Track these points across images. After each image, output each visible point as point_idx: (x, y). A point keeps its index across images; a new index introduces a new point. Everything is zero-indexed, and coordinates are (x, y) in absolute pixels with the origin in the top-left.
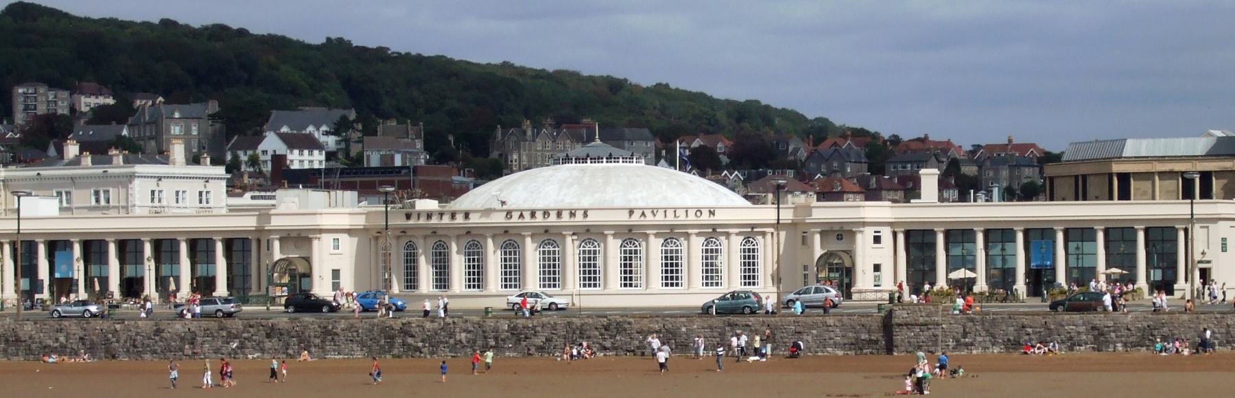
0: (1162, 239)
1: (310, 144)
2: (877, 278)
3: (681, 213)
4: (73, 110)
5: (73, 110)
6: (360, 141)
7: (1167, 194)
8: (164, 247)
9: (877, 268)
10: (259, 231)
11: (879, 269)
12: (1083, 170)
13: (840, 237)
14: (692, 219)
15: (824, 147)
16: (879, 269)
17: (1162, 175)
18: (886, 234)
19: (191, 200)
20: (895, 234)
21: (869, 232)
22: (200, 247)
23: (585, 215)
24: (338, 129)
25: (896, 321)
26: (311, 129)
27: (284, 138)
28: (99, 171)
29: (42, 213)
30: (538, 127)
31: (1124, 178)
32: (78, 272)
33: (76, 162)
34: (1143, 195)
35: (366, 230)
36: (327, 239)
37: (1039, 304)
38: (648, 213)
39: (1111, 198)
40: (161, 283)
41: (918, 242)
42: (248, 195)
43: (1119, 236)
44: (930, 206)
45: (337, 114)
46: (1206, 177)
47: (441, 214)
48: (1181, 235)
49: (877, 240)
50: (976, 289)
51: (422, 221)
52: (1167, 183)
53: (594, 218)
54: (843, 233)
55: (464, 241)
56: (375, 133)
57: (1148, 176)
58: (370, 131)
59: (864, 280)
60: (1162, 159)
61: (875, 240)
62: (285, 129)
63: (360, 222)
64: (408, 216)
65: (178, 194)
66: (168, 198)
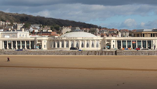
0: (150, 42)
1: (36, 29)
2: (114, 46)
3: (89, 38)
5: (5, 24)
6: (42, 28)
7: (149, 36)
8: (23, 42)
9: (114, 45)
10: (35, 40)
11: (114, 44)
12: (138, 33)
14: (85, 39)
15: (101, 30)
16: (114, 44)
17: (148, 34)
18: (115, 41)
20: (116, 41)
22: (28, 42)
23: (77, 38)
24: (40, 27)
25: (117, 52)
26: (36, 27)
27: (33, 28)
28: (13, 32)
29: (7, 37)
30: (65, 27)
31: (144, 34)
33: (10, 31)
34: (146, 37)
37: (15, 50)
38: (85, 38)
39: (142, 37)
40: (22, 46)
41: (119, 42)
42: (31, 35)
43: (144, 42)
44: (119, 37)
45: (39, 25)
46: (154, 34)
47: (58, 38)
48: (152, 41)
49: (114, 42)
51: (56, 39)
52: (149, 34)
53: (78, 39)
54: (109, 41)
55: (57, 41)
57: (147, 34)
58: (44, 27)
59: (112, 47)
60: (148, 32)
61: (113, 41)
62: (33, 27)
63: (48, 39)
64: (54, 38)
65: (24, 35)
66: (22, 36)
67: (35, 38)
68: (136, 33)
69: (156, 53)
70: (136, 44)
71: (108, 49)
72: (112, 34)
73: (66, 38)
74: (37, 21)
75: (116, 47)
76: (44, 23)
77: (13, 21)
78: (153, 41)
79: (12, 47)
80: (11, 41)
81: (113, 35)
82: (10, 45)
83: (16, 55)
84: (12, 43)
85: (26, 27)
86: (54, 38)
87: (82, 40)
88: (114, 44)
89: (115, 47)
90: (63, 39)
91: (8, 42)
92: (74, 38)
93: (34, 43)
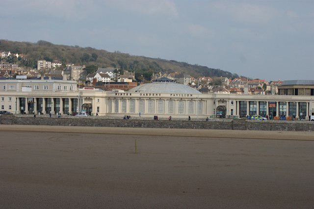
1: (107, 76)
3: (184, 95)
4: (52, 67)
5: (52, 67)
7: (307, 94)
9: (232, 110)
12: (286, 87)
13: (223, 102)
19: (68, 88)
21: (230, 101)
27: (100, 74)
31: (296, 90)
32: (52, 106)
33: (40, 78)
35: (106, 97)
36: (96, 99)
42: (84, 88)
48: (308, 104)
49: (232, 103)
50: (296, 117)
53: (162, 95)
56: (123, 74)
59: (228, 113)
62: (101, 72)
67: (81, 93)
68: (282, 88)
69: (310, 127)
70: (276, 108)
71: (221, 117)
72: (251, 89)
73: (138, 95)
74: (114, 62)
75: (236, 113)
76: (128, 66)
77: (68, 60)
78: (309, 103)
79: (35, 110)
80: (34, 99)
81: (254, 91)
82: (30, 105)
83: (247, 132)
84: (35, 101)
85: (88, 73)
86: (116, 94)
87: (171, 98)
88: (234, 107)
89: (234, 114)
90: (133, 95)
91: (28, 99)
92: (155, 95)
93: (307, 106)
